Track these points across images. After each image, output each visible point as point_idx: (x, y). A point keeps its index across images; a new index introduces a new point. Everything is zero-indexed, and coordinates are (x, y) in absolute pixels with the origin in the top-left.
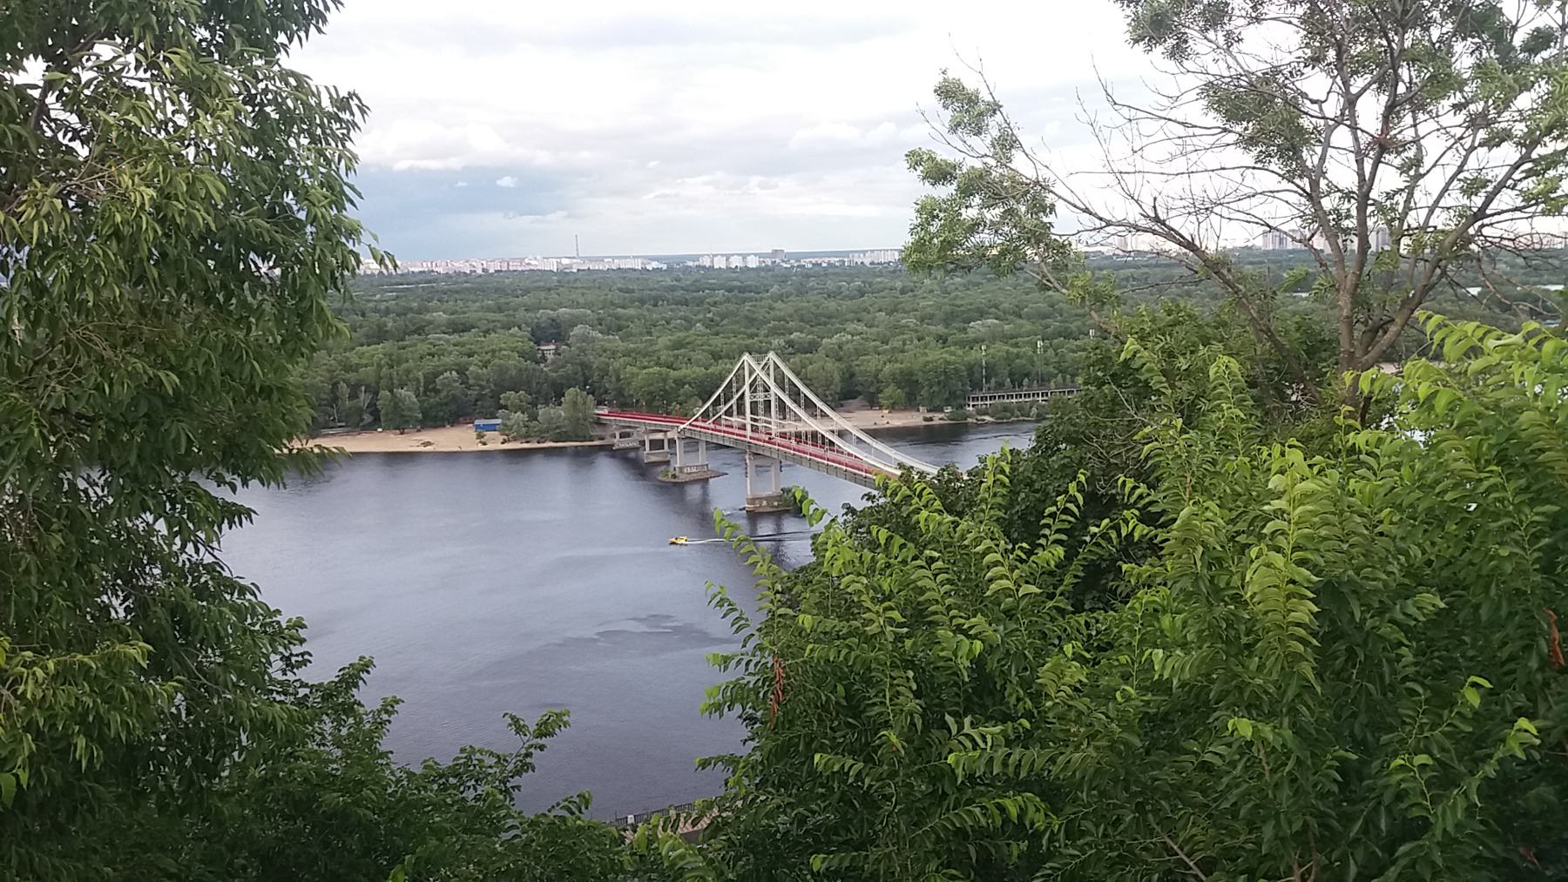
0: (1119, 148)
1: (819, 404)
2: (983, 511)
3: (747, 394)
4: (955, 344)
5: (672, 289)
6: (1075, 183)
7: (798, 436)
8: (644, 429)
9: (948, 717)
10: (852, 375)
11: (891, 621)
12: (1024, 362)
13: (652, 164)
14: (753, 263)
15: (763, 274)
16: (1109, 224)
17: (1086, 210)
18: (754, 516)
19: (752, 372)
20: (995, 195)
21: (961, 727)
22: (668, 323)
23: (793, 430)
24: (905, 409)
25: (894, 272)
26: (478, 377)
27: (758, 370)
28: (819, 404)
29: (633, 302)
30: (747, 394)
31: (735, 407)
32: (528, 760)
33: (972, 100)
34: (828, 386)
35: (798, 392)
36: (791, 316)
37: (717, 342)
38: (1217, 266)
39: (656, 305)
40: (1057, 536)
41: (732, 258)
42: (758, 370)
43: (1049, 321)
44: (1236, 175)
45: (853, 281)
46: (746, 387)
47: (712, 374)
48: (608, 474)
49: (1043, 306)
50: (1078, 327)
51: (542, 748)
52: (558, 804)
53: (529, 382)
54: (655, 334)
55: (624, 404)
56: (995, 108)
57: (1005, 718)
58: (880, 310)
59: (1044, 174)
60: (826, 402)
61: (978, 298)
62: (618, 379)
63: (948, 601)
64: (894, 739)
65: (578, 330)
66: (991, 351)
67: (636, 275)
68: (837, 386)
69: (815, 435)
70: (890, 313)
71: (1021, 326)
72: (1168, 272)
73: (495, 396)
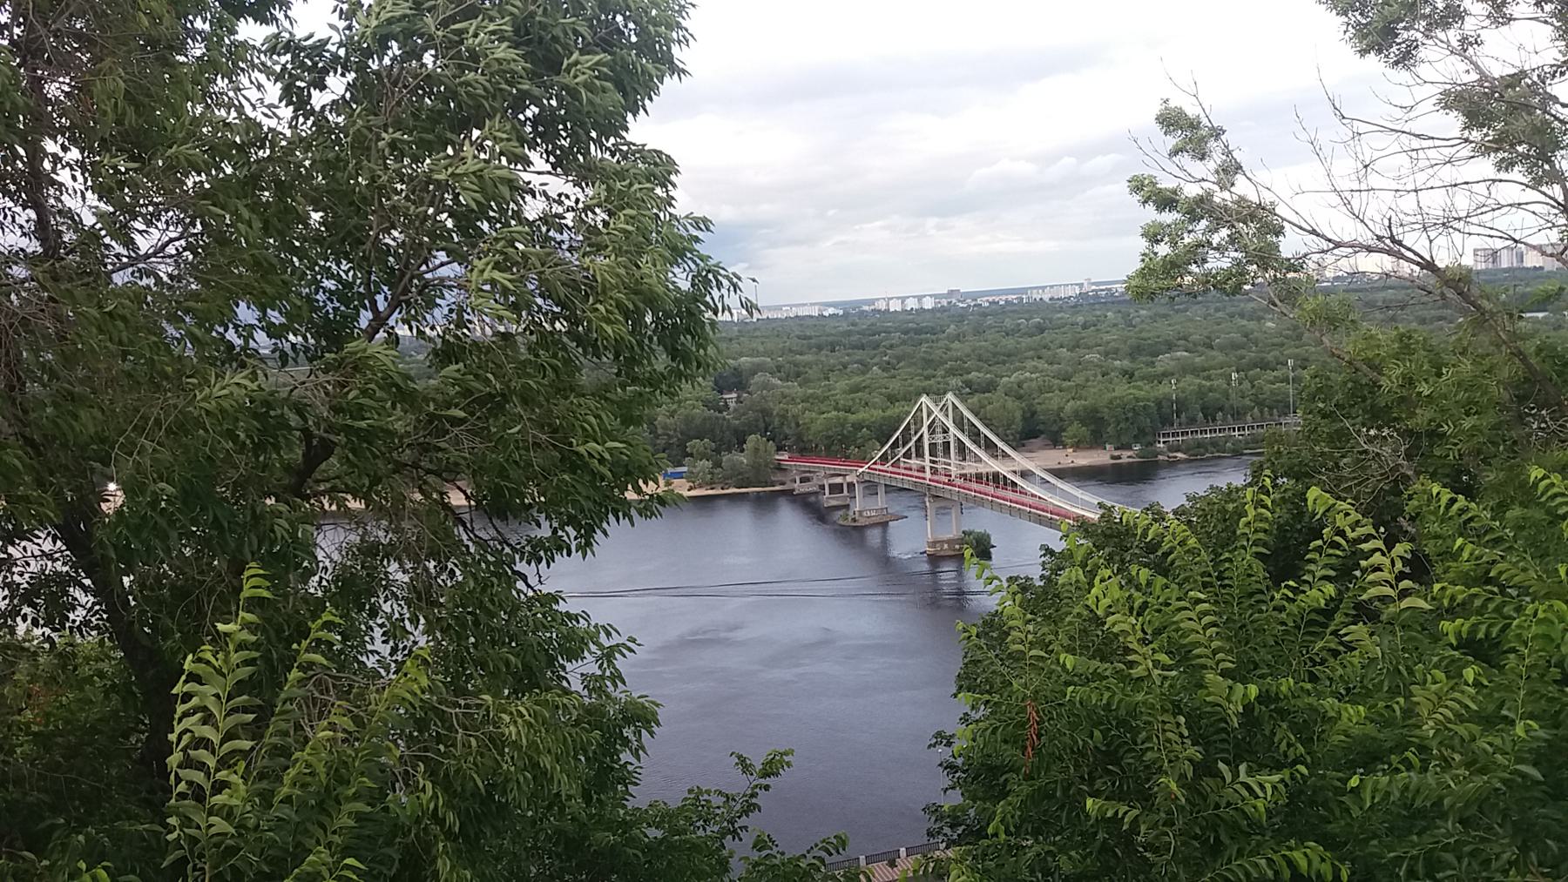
0: (1344, 168)
1: (1000, 444)
2: (1244, 548)
3: (926, 436)
4: (1142, 378)
5: (848, 333)
6: (1301, 204)
7: (979, 478)
8: (824, 473)
9: (1221, 765)
10: (1034, 413)
11: (1156, 663)
12: (1217, 396)
13: (831, 213)
14: (928, 304)
15: (938, 315)
16: (1338, 245)
17: (1314, 232)
18: (935, 559)
19: (930, 413)
20: (1220, 216)
21: (1236, 775)
22: (845, 368)
23: (973, 471)
24: (1091, 448)
25: (1075, 306)
26: (665, 427)
27: (936, 411)
28: (1000, 444)
29: (810, 348)
30: (926, 436)
31: (913, 450)
32: (754, 800)
33: (1194, 125)
34: (1009, 426)
35: (978, 433)
36: (968, 356)
37: (895, 386)
38: (1457, 282)
39: (833, 351)
40: (1324, 572)
41: (908, 301)
42: (936, 411)
43: (1243, 352)
44: (1481, 188)
45: (1032, 318)
46: (925, 429)
47: (890, 417)
48: (789, 520)
49: (1236, 336)
50: (1275, 357)
51: (767, 788)
52: (816, 845)
53: (713, 430)
54: (833, 379)
55: (804, 449)
56: (1217, 133)
57: (1277, 767)
58: (1062, 347)
59: (1267, 198)
60: (1007, 442)
61: (1165, 330)
62: (798, 425)
63: (1216, 644)
64: (1173, 786)
65: (758, 378)
66: (1181, 385)
67: (810, 322)
68: (1018, 425)
69: (996, 476)
70: (1071, 350)
71: (1214, 358)
72: (1370, 297)
73: (682, 445)
